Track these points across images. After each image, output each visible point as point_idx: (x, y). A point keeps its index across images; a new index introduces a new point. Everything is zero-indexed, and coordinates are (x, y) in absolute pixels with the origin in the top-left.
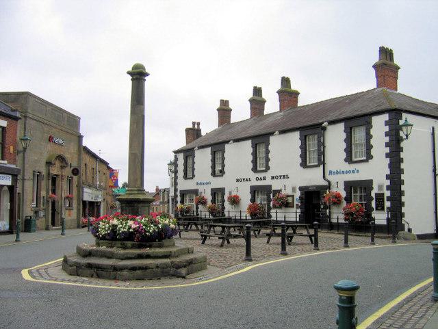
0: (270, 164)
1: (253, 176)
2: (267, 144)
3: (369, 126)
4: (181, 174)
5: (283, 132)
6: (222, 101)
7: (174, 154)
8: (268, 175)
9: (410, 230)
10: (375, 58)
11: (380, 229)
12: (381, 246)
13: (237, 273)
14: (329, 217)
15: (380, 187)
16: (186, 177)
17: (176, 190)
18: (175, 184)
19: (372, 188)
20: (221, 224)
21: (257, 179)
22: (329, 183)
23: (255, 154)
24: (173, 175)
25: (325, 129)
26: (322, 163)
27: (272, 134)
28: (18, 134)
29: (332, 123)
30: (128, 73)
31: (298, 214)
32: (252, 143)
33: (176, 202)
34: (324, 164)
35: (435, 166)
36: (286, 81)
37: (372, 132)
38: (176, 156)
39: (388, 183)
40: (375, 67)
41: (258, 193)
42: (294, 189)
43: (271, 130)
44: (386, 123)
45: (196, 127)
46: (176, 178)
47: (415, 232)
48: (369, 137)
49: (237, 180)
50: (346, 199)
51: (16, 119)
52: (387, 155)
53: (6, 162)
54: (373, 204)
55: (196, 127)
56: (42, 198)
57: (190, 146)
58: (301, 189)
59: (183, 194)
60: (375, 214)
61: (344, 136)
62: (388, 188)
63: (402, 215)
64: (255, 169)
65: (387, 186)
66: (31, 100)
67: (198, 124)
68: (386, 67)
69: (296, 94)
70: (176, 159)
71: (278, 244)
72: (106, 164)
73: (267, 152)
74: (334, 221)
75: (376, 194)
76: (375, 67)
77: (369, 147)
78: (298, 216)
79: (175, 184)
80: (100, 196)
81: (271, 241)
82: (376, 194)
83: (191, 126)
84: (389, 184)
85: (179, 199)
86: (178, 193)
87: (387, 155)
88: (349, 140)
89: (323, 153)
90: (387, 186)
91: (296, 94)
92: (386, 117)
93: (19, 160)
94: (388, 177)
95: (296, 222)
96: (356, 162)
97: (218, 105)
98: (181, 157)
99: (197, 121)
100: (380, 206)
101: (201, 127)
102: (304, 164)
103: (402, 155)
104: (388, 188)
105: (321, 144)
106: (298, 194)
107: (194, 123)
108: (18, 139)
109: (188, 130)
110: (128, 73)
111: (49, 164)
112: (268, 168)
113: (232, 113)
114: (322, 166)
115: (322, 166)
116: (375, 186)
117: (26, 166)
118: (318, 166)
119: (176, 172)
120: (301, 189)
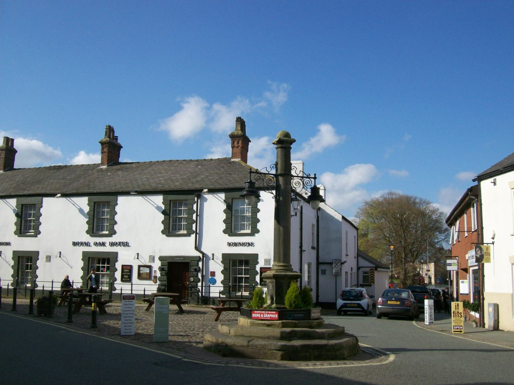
1: (86, 238)
8: (114, 239)
13: (126, 343)
15: (267, 261)
19: (258, 263)
20: (259, 312)
21: (96, 244)
29: (212, 191)
30: (294, 141)
32: (89, 201)
35: (301, 243)
42: (152, 259)
49: (138, 254)
54: (118, 275)
58: (161, 258)
68: (492, 182)
75: (261, 268)
82: (261, 268)
106: (157, 265)
110: (294, 141)
112: (113, 232)
120: (161, 258)
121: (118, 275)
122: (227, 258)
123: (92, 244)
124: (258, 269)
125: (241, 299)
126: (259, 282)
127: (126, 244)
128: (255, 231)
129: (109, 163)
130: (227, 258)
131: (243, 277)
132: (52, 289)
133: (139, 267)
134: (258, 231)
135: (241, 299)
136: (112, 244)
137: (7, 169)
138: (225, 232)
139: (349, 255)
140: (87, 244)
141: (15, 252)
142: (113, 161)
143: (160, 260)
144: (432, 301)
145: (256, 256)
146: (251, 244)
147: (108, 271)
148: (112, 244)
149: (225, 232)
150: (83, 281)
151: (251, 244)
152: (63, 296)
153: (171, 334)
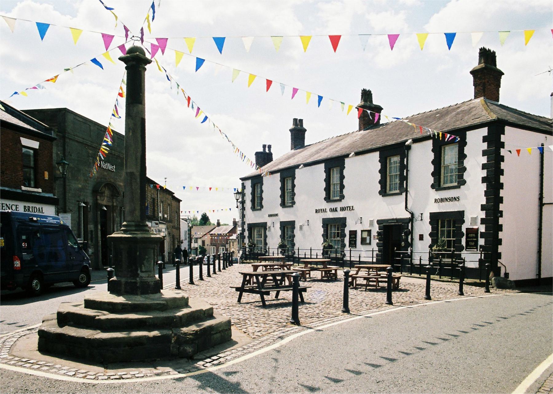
0: (345, 192)
1: (325, 205)
2: (342, 167)
3: (463, 144)
4: (248, 204)
5: (357, 154)
6: (295, 120)
7: (241, 182)
8: (343, 204)
9: (507, 275)
10: (475, 63)
11: (471, 273)
12: (456, 300)
14: (411, 256)
16: (253, 208)
17: (243, 223)
18: (243, 216)
19: (463, 222)
22: (412, 214)
23: (328, 180)
24: (240, 205)
25: (409, 148)
26: (403, 190)
27: (347, 156)
28: (54, 155)
29: (415, 141)
31: (375, 253)
33: (244, 237)
34: (406, 191)
36: (367, 95)
37: (467, 150)
38: (243, 184)
39: (483, 215)
40: (473, 72)
41: (331, 226)
42: (371, 223)
43: (344, 152)
44: (485, 139)
45: (267, 151)
46: (243, 209)
47: (512, 278)
48: (462, 156)
50: (235, 233)
51: (52, 139)
52: (484, 180)
53: (40, 190)
54: (347, 241)
55: (267, 151)
56: (89, 232)
57: (257, 172)
58: (379, 222)
59: (251, 227)
60: (465, 254)
61: (432, 156)
62: (483, 221)
63: (499, 256)
64: (328, 199)
65: (482, 219)
66: (70, 117)
67: (270, 147)
69: (379, 109)
70: (244, 187)
71: (267, 301)
72: (171, 193)
73: (342, 177)
74: (416, 262)
75: (467, 229)
76: (473, 72)
77: (462, 170)
78: (375, 255)
79: (243, 216)
80: (164, 230)
81: (243, 300)
82: (467, 229)
83: (261, 150)
84: (484, 217)
85: (246, 234)
86: (246, 227)
87: (484, 180)
88: (437, 162)
89: (406, 178)
90: (482, 219)
91: (379, 109)
92: (484, 131)
93: (58, 189)
94: (483, 208)
95: (373, 263)
96: (445, 189)
97: (291, 126)
98: (248, 184)
99: (267, 144)
100: (472, 244)
101: (272, 151)
102: (383, 192)
103: (502, 179)
104: (483, 221)
105: (404, 167)
106: (375, 229)
107: (264, 146)
108: (54, 163)
109: (257, 154)
111: (96, 192)
113: (307, 134)
114: (404, 194)
115: (404, 194)
116: (468, 218)
117: (69, 195)
118: (400, 194)
119: (243, 202)
120: (379, 222)
121: (347, 241)
122: (435, 218)
123: (328, 210)
124: (464, 230)
125: (252, 282)
126: (464, 245)
127: (351, 208)
128: (462, 182)
129: (367, 127)
130: (435, 218)
131: (451, 240)
132: (305, 256)
133: (362, 231)
134: (464, 183)
135: (252, 282)
136: (343, 209)
137: (297, 145)
138: (433, 186)
139: (384, 109)
140: (324, 211)
141: (281, 223)
142: (372, 124)
143: (379, 223)
144: (484, 66)
145: (461, 214)
146: (456, 199)
147: (338, 238)
148: (343, 209)
149: (433, 186)
150: (379, 249)
151: (456, 199)
152: (115, 270)
153: (457, 284)
